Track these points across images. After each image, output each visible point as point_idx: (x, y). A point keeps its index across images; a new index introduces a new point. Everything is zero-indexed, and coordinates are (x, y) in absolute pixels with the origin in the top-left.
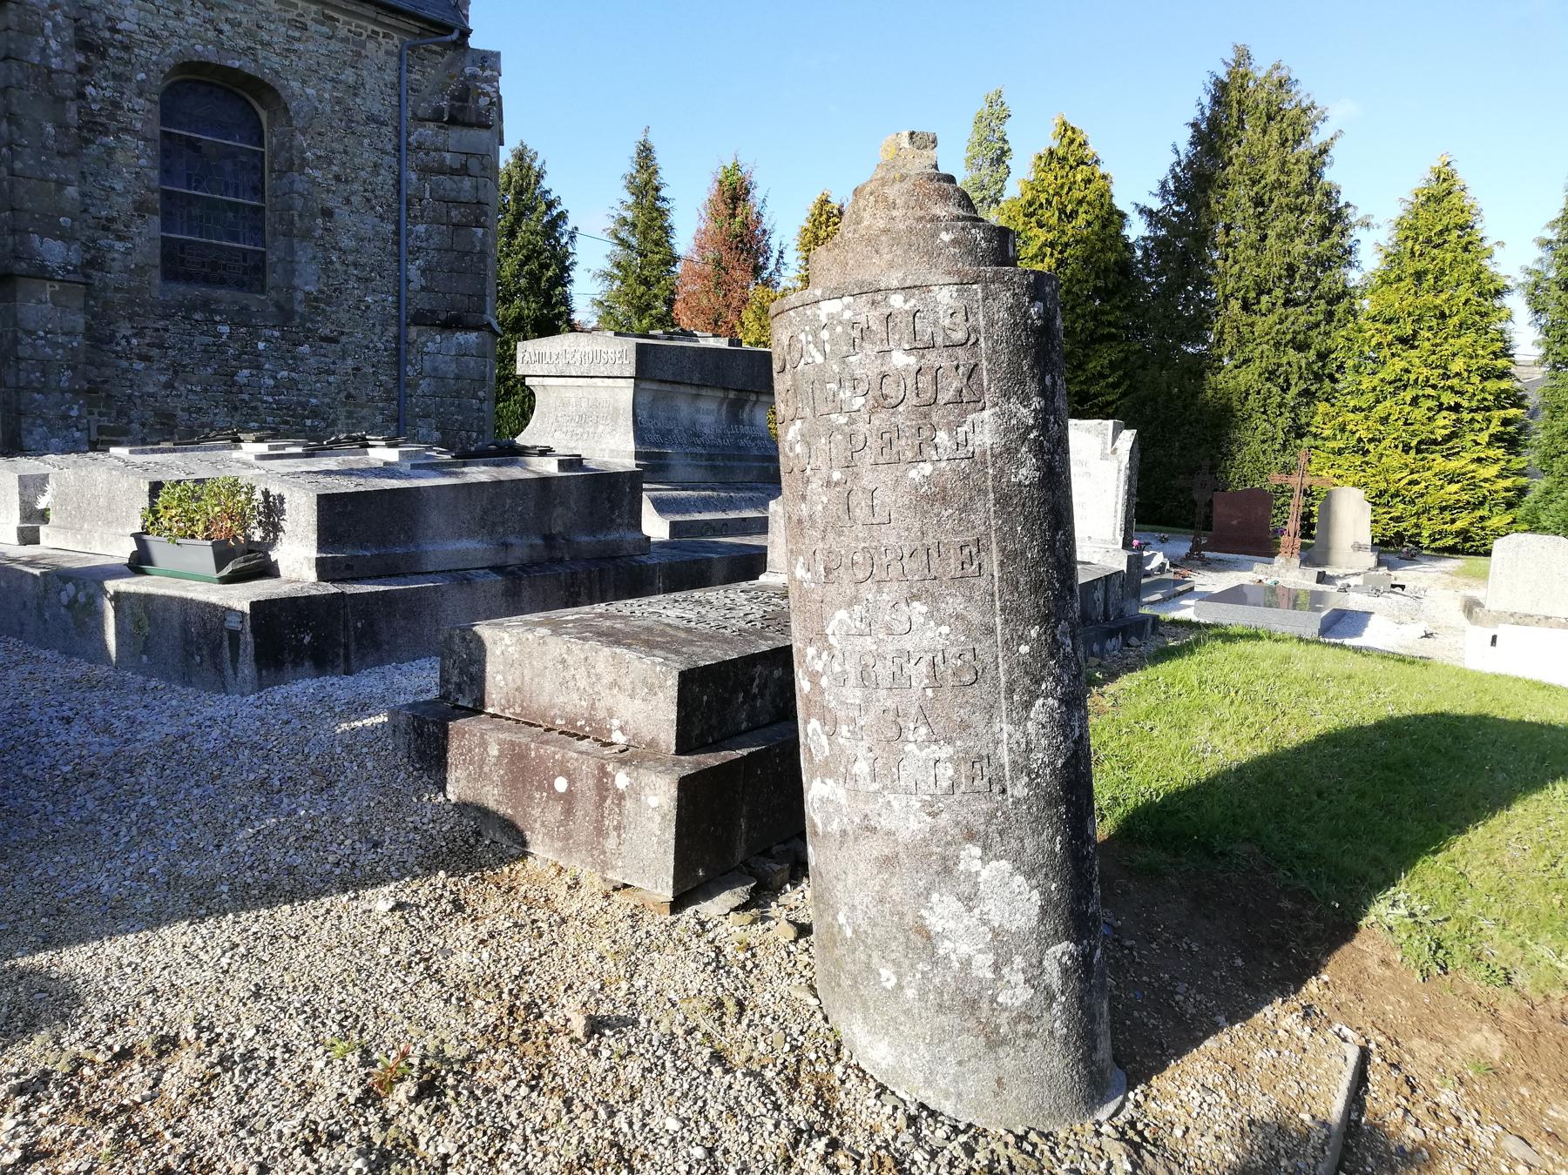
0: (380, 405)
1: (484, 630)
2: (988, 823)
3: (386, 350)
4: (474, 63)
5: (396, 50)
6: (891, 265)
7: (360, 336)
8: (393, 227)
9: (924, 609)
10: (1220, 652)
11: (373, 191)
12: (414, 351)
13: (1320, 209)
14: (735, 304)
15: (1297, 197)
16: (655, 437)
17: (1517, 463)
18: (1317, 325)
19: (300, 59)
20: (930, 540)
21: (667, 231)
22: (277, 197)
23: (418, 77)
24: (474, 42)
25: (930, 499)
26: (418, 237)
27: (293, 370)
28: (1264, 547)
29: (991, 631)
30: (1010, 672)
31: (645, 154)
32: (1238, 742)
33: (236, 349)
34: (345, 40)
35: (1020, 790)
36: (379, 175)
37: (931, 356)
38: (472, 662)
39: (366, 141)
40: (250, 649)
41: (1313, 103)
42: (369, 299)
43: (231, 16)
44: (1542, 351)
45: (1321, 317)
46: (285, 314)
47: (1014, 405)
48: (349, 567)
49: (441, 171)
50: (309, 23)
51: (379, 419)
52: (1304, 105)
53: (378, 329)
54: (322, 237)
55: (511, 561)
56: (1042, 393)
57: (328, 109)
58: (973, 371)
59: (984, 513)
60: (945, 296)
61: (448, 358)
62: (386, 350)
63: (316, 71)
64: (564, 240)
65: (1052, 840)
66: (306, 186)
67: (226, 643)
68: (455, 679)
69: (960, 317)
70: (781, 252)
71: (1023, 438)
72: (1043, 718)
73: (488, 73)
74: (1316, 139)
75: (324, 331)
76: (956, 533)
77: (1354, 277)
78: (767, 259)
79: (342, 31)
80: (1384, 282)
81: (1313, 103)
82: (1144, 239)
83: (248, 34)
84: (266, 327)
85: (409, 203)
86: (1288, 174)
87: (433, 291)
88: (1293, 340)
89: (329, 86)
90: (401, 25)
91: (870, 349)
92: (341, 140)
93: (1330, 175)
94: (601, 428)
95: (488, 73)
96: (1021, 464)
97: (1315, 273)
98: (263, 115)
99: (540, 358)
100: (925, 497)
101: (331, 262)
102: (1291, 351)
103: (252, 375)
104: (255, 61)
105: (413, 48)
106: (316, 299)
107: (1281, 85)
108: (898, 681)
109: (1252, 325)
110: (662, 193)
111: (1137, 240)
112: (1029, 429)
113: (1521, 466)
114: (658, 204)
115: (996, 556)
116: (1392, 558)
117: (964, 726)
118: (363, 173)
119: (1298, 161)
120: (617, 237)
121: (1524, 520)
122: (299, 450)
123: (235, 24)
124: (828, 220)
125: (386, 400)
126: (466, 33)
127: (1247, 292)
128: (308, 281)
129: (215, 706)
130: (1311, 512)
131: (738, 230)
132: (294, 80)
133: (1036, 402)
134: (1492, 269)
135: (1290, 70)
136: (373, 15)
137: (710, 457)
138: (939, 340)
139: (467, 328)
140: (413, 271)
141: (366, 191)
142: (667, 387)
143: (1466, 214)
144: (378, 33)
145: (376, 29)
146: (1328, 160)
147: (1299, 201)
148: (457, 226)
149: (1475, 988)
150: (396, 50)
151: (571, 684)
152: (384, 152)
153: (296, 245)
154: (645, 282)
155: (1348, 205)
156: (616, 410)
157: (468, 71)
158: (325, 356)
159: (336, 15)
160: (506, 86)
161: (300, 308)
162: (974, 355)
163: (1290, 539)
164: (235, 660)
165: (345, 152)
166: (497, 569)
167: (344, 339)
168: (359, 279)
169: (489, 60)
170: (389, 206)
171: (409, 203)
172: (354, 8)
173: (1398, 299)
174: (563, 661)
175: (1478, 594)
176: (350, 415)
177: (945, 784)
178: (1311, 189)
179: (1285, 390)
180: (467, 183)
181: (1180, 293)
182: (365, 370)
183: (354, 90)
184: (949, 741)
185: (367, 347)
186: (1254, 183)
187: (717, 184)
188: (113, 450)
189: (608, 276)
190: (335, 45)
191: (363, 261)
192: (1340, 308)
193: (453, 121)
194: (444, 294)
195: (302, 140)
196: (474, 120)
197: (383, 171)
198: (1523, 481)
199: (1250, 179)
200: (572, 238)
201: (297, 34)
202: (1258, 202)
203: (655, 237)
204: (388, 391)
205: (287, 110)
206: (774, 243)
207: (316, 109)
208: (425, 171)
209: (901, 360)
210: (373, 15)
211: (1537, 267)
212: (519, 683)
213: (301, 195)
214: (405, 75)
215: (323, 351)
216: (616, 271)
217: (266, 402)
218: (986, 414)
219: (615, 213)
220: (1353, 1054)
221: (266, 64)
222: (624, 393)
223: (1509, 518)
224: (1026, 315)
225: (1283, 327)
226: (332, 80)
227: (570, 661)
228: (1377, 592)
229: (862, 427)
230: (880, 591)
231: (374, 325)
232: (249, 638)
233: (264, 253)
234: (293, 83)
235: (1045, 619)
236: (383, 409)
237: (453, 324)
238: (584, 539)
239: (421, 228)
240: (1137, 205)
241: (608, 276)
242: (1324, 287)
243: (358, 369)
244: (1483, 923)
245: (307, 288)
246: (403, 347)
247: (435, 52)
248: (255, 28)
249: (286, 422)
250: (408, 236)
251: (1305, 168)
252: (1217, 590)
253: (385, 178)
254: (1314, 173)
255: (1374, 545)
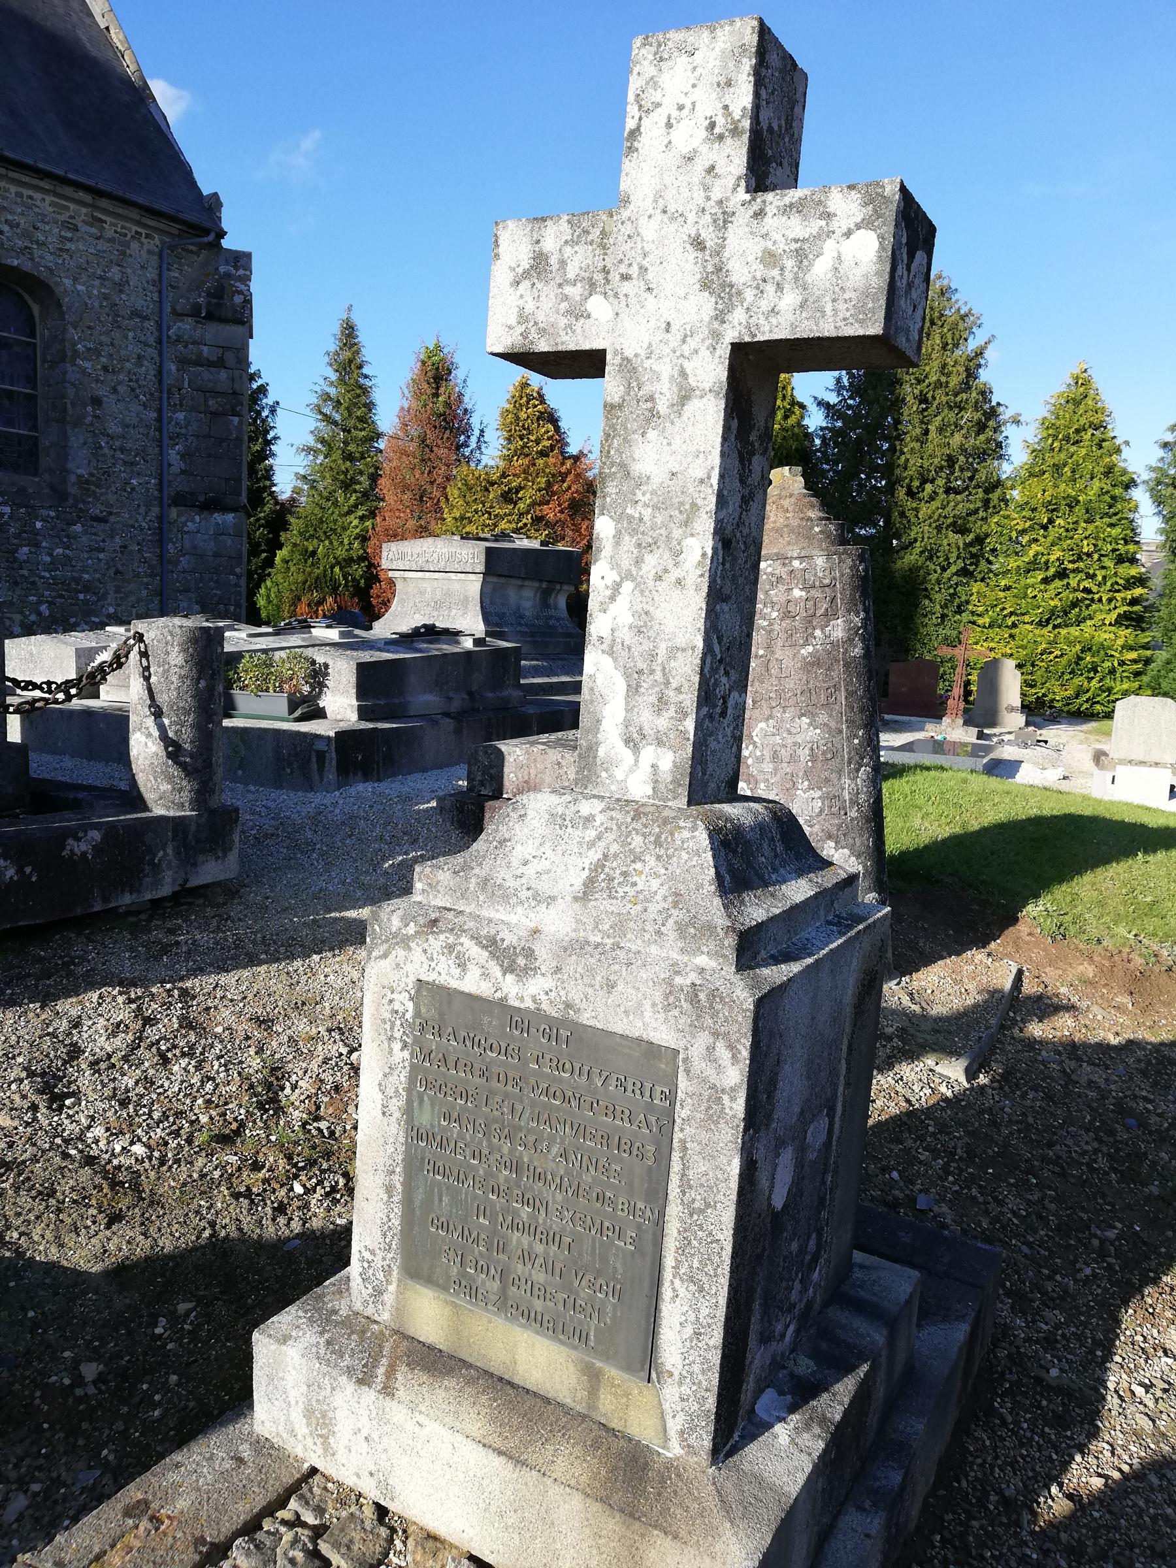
0: (145, 580)
1: (505, 746)
2: (838, 830)
3: (149, 529)
4: (227, 263)
5: (156, 250)
6: (789, 543)
7: (127, 516)
8: (155, 415)
9: (808, 721)
10: (920, 777)
11: (137, 381)
12: (175, 530)
13: (976, 408)
14: (439, 480)
15: (956, 395)
16: (495, 619)
17: (1145, 638)
18: (976, 511)
19: (71, 257)
20: (810, 686)
21: (370, 406)
22: (49, 386)
23: (177, 275)
24: (226, 243)
25: (812, 664)
26: (177, 424)
27: (67, 548)
28: (934, 710)
29: (841, 732)
30: (849, 753)
31: (349, 333)
32: (940, 826)
33: (16, 528)
34: (111, 240)
35: (853, 813)
36: (142, 366)
37: (813, 592)
38: (491, 766)
39: (131, 334)
40: (334, 762)
41: (970, 310)
42: (134, 482)
43: (10, 217)
44: (1163, 538)
45: (979, 504)
46: (59, 495)
47: (852, 616)
48: (373, 712)
49: (199, 362)
50: (80, 225)
51: (144, 593)
52: (962, 312)
53: (142, 510)
54: (92, 424)
55: (453, 710)
56: (864, 610)
57: (96, 304)
58: (833, 599)
59: (839, 671)
60: (820, 561)
61: (207, 537)
62: (149, 529)
63: (86, 269)
64: (265, 413)
65: (868, 840)
66: (78, 376)
67: (314, 759)
68: (479, 778)
69: (827, 572)
70: (482, 431)
71: (857, 633)
72: (864, 777)
73: (241, 272)
74: (972, 345)
75: (95, 511)
76: (825, 682)
77: (1006, 470)
78: (469, 437)
79: (109, 233)
80: (1031, 475)
81: (970, 310)
82: (822, 429)
83: (26, 235)
84: (42, 507)
85: (169, 392)
86: (948, 375)
87: (192, 474)
88: (954, 524)
89: (97, 283)
90: (162, 226)
91: (782, 588)
92: (108, 333)
93: (985, 376)
94: (454, 612)
95: (241, 272)
96: (855, 646)
97: (972, 464)
98: (36, 309)
99: (402, 556)
100: (809, 663)
101: (101, 447)
102: (951, 534)
103: (31, 553)
104: (32, 259)
105: (172, 248)
106: (87, 482)
107: (943, 294)
108: (793, 759)
109: (917, 510)
110: (365, 371)
111: (816, 430)
112: (859, 629)
113: (1146, 640)
114: (361, 381)
115: (843, 694)
116: (1038, 720)
117: (827, 780)
118: (128, 364)
119: (956, 362)
120: (321, 413)
121: (1148, 686)
122: (270, 630)
123: (13, 225)
124: (528, 403)
125: (150, 576)
126: (222, 234)
127: (911, 480)
128: (80, 466)
129: (318, 799)
130: (969, 681)
131: (441, 410)
132: (66, 277)
133: (862, 615)
134: (1122, 464)
135: (950, 280)
136: (137, 217)
137: (532, 635)
138: (817, 584)
139: (225, 509)
140: (173, 455)
141: (130, 380)
142: (503, 580)
143: (1100, 415)
144: (140, 234)
145: (140, 230)
146: (983, 362)
147: (958, 399)
148: (214, 414)
149: (1081, 946)
150: (156, 250)
151: (564, 777)
152: (146, 344)
153: (69, 431)
154: (349, 457)
155: (999, 404)
156: (466, 598)
157: (222, 269)
158: (95, 534)
159: (103, 217)
160: (257, 287)
161: (73, 490)
162: (834, 591)
163: (955, 702)
164: (321, 770)
165: (112, 344)
166: (446, 715)
167: (112, 519)
168: (125, 463)
169: (242, 260)
170: (151, 395)
171: (169, 392)
172: (120, 211)
173: (1041, 491)
174: (559, 763)
175: (1104, 747)
176: (118, 590)
177: (817, 810)
178: (966, 387)
179: (944, 569)
180: (223, 374)
181: (853, 480)
182: (131, 548)
183: (120, 286)
184: (820, 788)
185: (133, 526)
186: (919, 382)
187: (419, 364)
188: (108, 628)
189: (309, 450)
190: (102, 245)
191: (128, 446)
192: (995, 496)
193: (210, 317)
194: (202, 477)
195: (73, 334)
196: (230, 316)
197: (146, 363)
198: (1148, 653)
199: (916, 379)
200: (273, 411)
201: (69, 235)
202: (923, 399)
203: (359, 414)
204: (151, 567)
205: (59, 305)
206: (475, 421)
207: (86, 304)
208: (183, 362)
209: (797, 593)
210: (137, 217)
211: (1160, 465)
212: (526, 778)
213: (74, 385)
214: (166, 273)
215: (93, 530)
216: (320, 446)
217: (43, 577)
218: (839, 621)
219: (318, 389)
220: (1014, 971)
221: (43, 262)
222: (474, 585)
223: (1136, 684)
224: (858, 570)
225: (945, 512)
226: (100, 277)
227: (564, 763)
228: (1026, 746)
229: (776, 627)
230: (784, 712)
231: (139, 506)
232: (334, 755)
233: (37, 437)
234: (66, 281)
235: (865, 727)
236: (147, 584)
237: (212, 505)
238: (490, 695)
239: (180, 416)
240: (816, 398)
241: (309, 450)
242: (982, 476)
243: (125, 547)
244: (1087, 916)
245: (79, 471)
246: (166, 526)
247: (191, 252)
248: (31, 229)
249: (62, 596)
250: (169, 423)
251: (962, 369)
252: (897, 744)
253: (148, 369)
254: (971, 374)
255: (1023, 706)
